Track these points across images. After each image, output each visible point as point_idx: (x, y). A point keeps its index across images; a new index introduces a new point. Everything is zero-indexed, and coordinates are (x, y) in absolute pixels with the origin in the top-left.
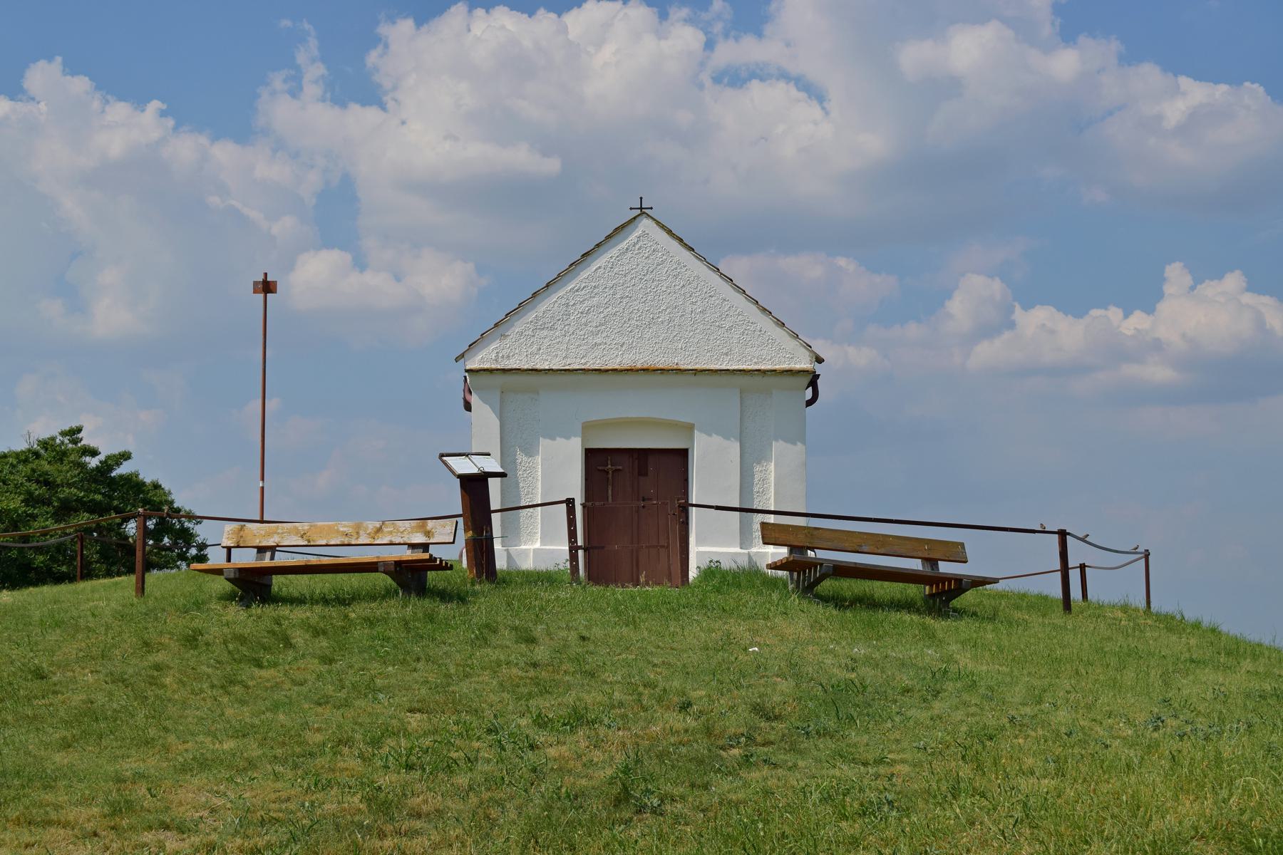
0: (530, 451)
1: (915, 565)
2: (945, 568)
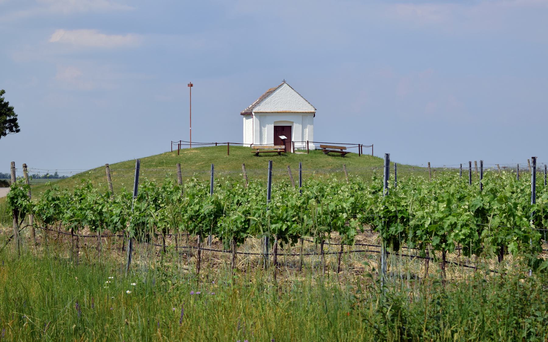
0: (264, 127)
1: (339, 150)
2: (344, 151)
